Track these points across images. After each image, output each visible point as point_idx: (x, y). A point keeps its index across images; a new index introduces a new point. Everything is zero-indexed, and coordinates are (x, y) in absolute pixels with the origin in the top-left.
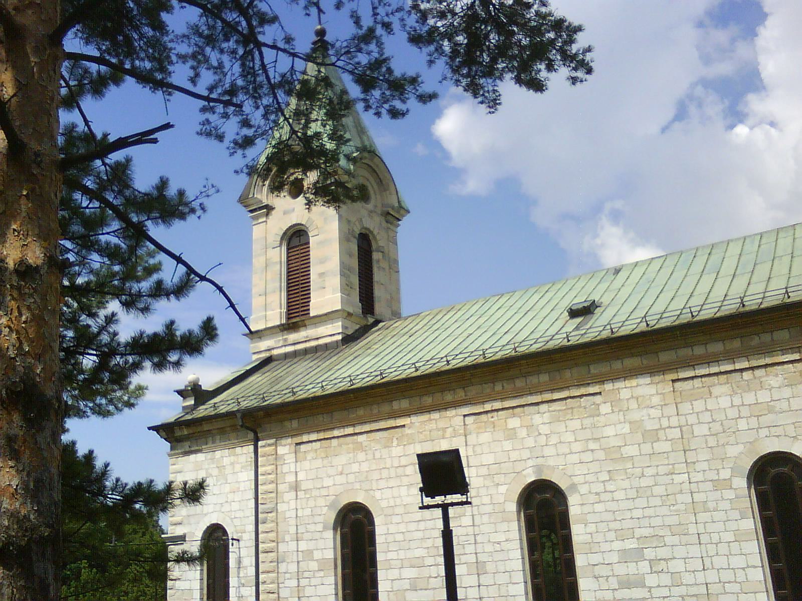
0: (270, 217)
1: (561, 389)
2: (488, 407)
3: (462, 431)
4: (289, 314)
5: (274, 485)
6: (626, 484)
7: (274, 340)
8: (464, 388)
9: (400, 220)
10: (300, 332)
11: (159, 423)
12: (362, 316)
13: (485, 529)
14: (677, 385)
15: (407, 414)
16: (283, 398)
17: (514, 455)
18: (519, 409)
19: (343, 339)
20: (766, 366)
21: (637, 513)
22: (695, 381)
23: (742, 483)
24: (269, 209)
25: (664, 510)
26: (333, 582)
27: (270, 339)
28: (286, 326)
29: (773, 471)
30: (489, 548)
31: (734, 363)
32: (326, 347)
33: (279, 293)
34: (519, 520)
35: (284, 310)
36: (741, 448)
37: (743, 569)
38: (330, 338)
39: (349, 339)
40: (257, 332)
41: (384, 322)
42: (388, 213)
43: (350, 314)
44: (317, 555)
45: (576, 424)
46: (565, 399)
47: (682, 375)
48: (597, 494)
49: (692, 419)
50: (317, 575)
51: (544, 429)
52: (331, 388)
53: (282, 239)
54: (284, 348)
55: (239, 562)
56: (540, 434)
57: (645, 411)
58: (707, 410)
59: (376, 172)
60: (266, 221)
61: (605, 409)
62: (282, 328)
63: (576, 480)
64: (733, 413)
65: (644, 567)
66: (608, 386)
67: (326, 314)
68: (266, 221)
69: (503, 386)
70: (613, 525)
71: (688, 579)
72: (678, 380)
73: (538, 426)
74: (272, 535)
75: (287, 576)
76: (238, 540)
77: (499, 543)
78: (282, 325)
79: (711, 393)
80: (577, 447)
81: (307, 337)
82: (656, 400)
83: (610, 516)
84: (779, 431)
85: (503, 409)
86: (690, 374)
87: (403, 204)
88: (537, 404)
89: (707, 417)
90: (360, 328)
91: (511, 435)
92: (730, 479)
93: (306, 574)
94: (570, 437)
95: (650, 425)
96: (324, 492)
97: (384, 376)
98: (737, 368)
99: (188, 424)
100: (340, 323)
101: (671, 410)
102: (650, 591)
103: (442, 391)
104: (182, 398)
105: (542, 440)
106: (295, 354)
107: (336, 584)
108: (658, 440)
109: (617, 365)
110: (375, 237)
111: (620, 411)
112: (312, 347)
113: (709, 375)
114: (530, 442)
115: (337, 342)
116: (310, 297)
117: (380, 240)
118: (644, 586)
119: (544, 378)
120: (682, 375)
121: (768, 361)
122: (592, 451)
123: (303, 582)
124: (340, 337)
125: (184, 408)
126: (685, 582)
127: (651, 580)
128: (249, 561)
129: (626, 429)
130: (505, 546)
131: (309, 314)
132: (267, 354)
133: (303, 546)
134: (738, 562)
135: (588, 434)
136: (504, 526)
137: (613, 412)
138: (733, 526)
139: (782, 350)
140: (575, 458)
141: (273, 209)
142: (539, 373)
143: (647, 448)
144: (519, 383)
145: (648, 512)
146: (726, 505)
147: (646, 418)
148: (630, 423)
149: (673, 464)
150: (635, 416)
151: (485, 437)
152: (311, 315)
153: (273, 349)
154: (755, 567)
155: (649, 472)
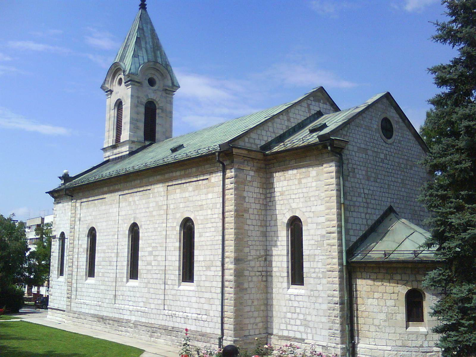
0: (112, 95)
2: (125, 192)
4: (117, 140)
5: (74, 218)
7: (110, 152)
9: (175, 92)
14: (169, 188)
16: (292, 146)
19: (129, 153)
20: (189, 182)
21: (153, 238)
23: (178, 228)
31: (197, 177)
42: (166, 90)
43: (133, 142)
52: (315, 139)
53: (115, 106)
55: (67, 247)
59: (159, 70)
63: (143, 223)
66: (153, 187)
68: (110, 97)
79: (176, 192)
80: (144, 210)
81: (119, 152)
84: (189, 209)
86: (195, 179)
87: (175, 84)
92: (176, 227)
96: (86, 222)
97: (304, 141)
98: (182, 182)
100: (128, 146)
104: (61, 180)
110: (157, 102)
117: (160, 103)
118: (151, 265)
121: (190, 180)
124: (128, 153)
125: (61, 184)
126: (160, 265)
131: (120, 141)
132: (107, 159)
139: (203, 174)
140: (143, 215)
141: (113, 91)
145: (156, 237)
150: (157, 199)
154: (177, 261)
155: (158, 222)
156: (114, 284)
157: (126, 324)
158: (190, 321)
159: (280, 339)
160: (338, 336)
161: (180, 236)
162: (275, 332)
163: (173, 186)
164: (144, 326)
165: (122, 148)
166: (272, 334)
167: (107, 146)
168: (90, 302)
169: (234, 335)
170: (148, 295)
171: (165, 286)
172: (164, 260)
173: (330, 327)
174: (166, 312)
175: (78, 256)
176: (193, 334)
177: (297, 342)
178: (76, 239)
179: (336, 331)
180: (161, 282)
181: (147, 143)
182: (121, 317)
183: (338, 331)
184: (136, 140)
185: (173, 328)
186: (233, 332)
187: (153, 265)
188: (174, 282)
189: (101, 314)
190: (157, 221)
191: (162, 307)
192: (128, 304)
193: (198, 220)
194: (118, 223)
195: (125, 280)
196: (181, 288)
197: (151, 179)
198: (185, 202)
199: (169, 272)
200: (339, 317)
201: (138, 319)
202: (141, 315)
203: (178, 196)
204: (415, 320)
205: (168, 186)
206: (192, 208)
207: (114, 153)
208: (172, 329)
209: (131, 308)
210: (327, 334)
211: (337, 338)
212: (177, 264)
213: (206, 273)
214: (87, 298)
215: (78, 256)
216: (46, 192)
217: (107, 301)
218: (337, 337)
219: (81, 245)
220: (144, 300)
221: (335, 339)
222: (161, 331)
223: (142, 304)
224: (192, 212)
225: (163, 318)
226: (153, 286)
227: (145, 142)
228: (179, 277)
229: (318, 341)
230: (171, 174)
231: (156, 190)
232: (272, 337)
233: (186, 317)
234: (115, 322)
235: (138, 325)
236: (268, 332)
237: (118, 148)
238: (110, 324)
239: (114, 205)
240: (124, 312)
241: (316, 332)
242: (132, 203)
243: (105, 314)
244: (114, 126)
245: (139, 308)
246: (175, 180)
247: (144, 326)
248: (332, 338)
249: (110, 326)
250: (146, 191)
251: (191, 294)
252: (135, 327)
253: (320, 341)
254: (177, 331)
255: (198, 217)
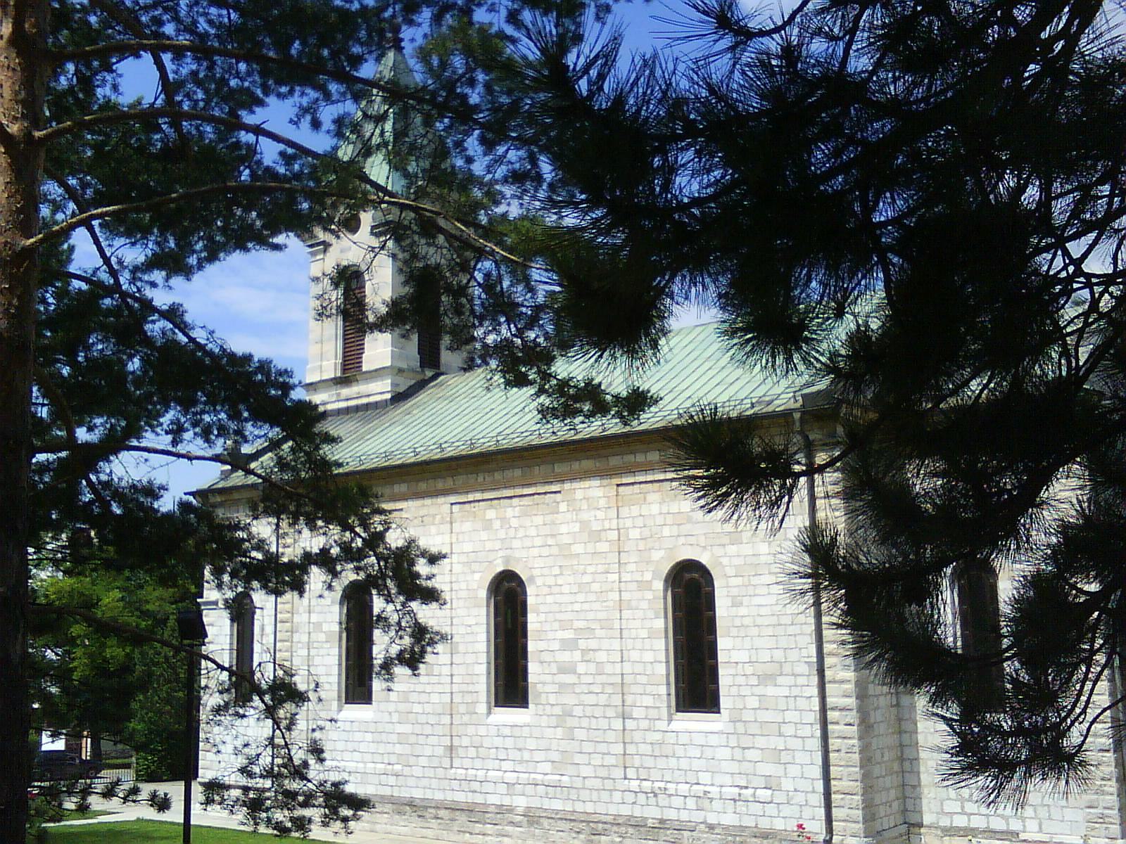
0: (328, 254)
1: (529, 485)
2: (471, 497)
3: (449, 519)
4: (345, 365)
6: (571, 579)
8: (452, 477)
10: (351, 386)
11: (195, 490)
12: (419, 369)
13: (460, 612)
14: (621, 489)
15: (404, 498)
17: (489, 545)
18: (496, 502)
19: (392, 398)
21: (577, 607)
22: (635, 486)
23: (659, 585)
24: (326, 245)
25: (596, 606)
26: (337, 653)
27: (325, 393)
28: (338, 380)
29: (687, 576)
30: (462, 630)
32: (376, 405)
33: (334, 342)
34: (488, 606)
35: (340, 361)
36: (662, 553)
37: (651, 663)
38: (380, 396)
39: (399, 398)
40: (311, 384)
41: (446, 374)
43: (400, 371)
44: (325, 627)
45: (539, 520)
46: (533, 494)
47: (625, 481)
48: (550, 587)
49: (629, 523)
50: (325, 646)
51: (514, 523)
54: (337, 403)
55: (263, 630)
56: (511, 527)
57: (593, 513)
58: (641, 515)
60: (323, 259)
61: (563, 507)
62: (334, 381)
63: (536, 572)
64: (659, 520)
65: (577, 655)
66: (567, 486)
67: (376, 370)
68: (323, 259)
69: (484, 478)
70: (559, 616)
71: (608, 669)
72: (622, 485)
73: (509, 519)
74: (288, 607)
75: (300, 645)
76: (262, 608)
77: (470, 626)
78: (335, 379)
80: (538, 541)
81: (359, 393)
82: (602, 503)
83: (556, 608)
84: (692, 540)
85: (483, 500)
88: (510, 498)
89: (640, 522)
90: (415, 384)
91: (488, 525)
92: (651, 581)
93: (315, 645)
94: (533, 532)
95: (596, 526)
98: (667, 478)
99: (222, 491)
100: (389, 381)
101: (613, 513)
102: (579, 678)
103: (434, 478)
105: (512, 533)
106: (347, 410)
107: (340, 656)
108: (600, 541)
109: (576, 466)
111: (574, 510)
112: (363, 405)
113: (646, 482)
114: (502, 534)
115: (386, 401)
116: (363, 349)
118: (575, 673)
119: (518, 472)
120: (625, 481)
122: (549, 546)
123: (313, 652)
124: (388, 396)
126: (606, 671)
127: (581, 668)
128: (269, 629)
129: (577, 527)
130: (475, 629)
133: (314, 618)
134: (649, 656)
135: (546, 530)
136: (475, 611)
137: (568, 511)
138: (648, 624)
140: (535, 552)
141: (331, 245)
142: (513, 467)
143: (590, 547)
144: (498, 476)
145: (586, 606)
146: (644, 605)
147: (593, 519)
148: (580, 522)
149: (609, 564)
150: (585, 516)
151: (467, 526)
152: (364, 369)
153: (328, 403)
154: (661, 662)
155: (591, 569)
156: (446, 720)
157: (499, 816)
158: (717, 805)
159: (946, 835)
160: (1115, 821)
161: (665, 603)
162: (927, 819)
163: (636, 486)
164: (561, 819)
165: (368, 383)
166: (920, 825)
167: (319, 379)
168: (361, 765)
169: (865, 832)
170: (565, 745)
171: (624, 722)
172: (619, 660)
173: (1091, 801)
174: (634, 785)
175: (309, 652)
176: (731, 835)
177: (998, 839)
178: (301, 609)
179: (1107, 812)
180: (610, 712)
181: (429, 373)
182: (479, 799)
183: (1112, 809)
184: (404, 366)
185: (662, 821)
186: (861, 825)
187: (579, 672)
188: (653, 713)
189: (405, 794)
190: (588, 567)
191: (618, 773)
192: (498, 768)
193: (724, 567)
194: (451, 571)
195: (482, 708)
196: (675, 725)
197: (558, 468)
198: (679, 525)
199: (634, 689)
200: (1114, 780)
201: (535, 803)
202: (547, 793)
203: (655, 509)
204: (55, 754)
205: (618, 485)
206: (703, 538)
207: (342, 397)
208: (660, 823)
209: (511, 777)
210: (1080, 818)
211: (1109, 826)
212: (661, 669)
213: (760, 690)
214: (347, 756)
215: (309, 652)
216: (186, 491)
217: (423, 761)
218: (1111, 823)
219: (318, 625)
220: (555, 756)
221: (1106, 828)
222: (623, 829)
223: (547, 767)
224: (704, 547)
225: (623, 799)
226: (585, 722)
227: (423, 371)
228: (669, 701)
229: (1056, 834)
230: (630, 458)
231: (579, 494)
232: (922, 830)
233: (702, 795)
234: (458, 813)
235: (540, 817)
236: (907, 820)
237: (353, 384)
238: (442, 819)
239: (432, 527)
240: (488, 787)
241: (1050, 815)
242: (497, 524)
243: (418, 794)
244: (337, 329)
245: (539, 777)
246: (651, 472)
247: (561, 819)
248: (1097, 825)
249: (440, 824)
250: (543, 496)
251: (713, 740)
252: (531, 823)
253: (1061, 834)
254: (679, 828)
255: (725, 561)
